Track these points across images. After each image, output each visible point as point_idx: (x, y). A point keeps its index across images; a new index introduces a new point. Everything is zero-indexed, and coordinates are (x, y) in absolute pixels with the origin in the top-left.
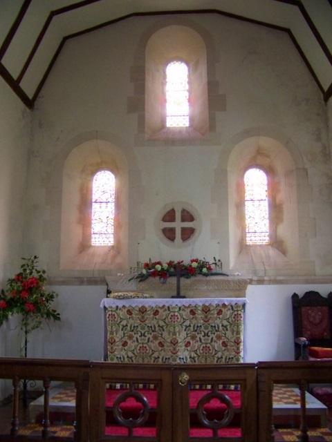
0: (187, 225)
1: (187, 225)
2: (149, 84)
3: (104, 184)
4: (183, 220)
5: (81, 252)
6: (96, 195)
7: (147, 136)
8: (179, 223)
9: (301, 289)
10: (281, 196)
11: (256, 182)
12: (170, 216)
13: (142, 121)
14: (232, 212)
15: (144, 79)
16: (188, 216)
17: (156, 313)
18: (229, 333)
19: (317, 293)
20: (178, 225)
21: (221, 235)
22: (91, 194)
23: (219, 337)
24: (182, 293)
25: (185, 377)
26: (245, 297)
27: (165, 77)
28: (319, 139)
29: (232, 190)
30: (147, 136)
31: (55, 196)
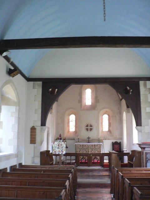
0: (91, 128)
1: (91, 128)
2: (83, 97)
3: (72, 118)
4: (90, 127)
5: (111, 133)
6: (71, 119)
7: (82, 108)
8: (89, 128)
9: (114, 141)
10: (111, 121)
11: (105, 118)
12: (87, 126)
13: (81, 104)
14: (100, 125)
15: (82, 95)
16: (91, 126)
17: (85, 146)
18: (99, 150)
19: (117, 142)
20: (89, 128)
21: (98, 130)
22: (123, 147)
23: (97, 150)
24: (90, 142)
25: (91, 155)
26: (121, 164)
27: (86, 93)
28: (119, 109)
29: (100, 119)
30: (82, 108)
31: (63, 122)
